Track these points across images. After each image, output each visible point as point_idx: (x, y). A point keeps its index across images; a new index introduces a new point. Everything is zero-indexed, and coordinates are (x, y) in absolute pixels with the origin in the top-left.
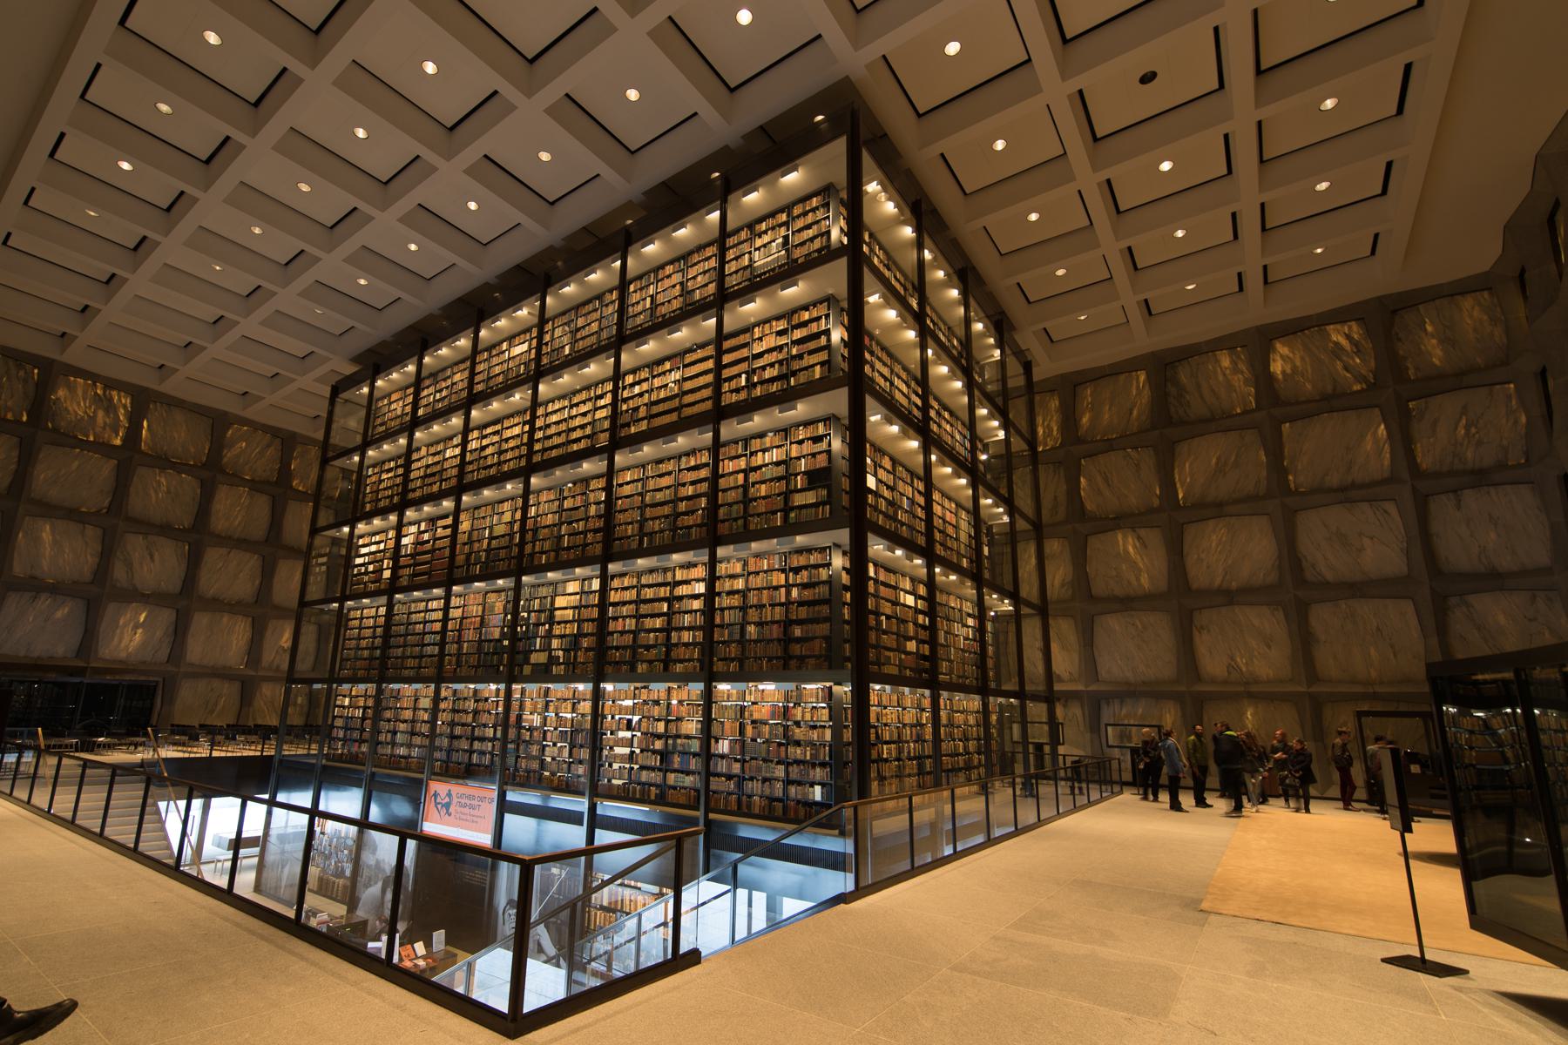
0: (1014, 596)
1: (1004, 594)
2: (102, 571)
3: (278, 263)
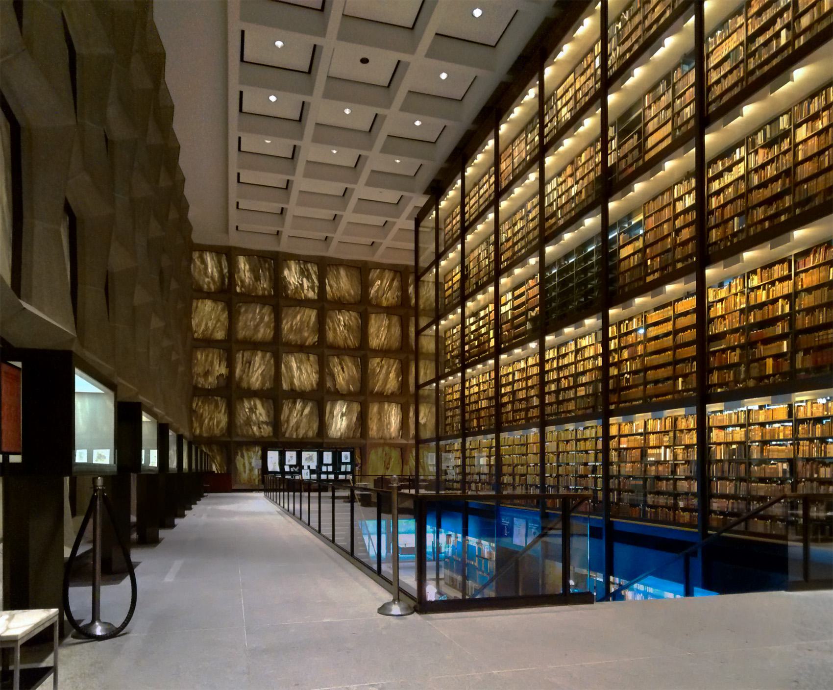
2: (321, 382)
3: (337, 196)
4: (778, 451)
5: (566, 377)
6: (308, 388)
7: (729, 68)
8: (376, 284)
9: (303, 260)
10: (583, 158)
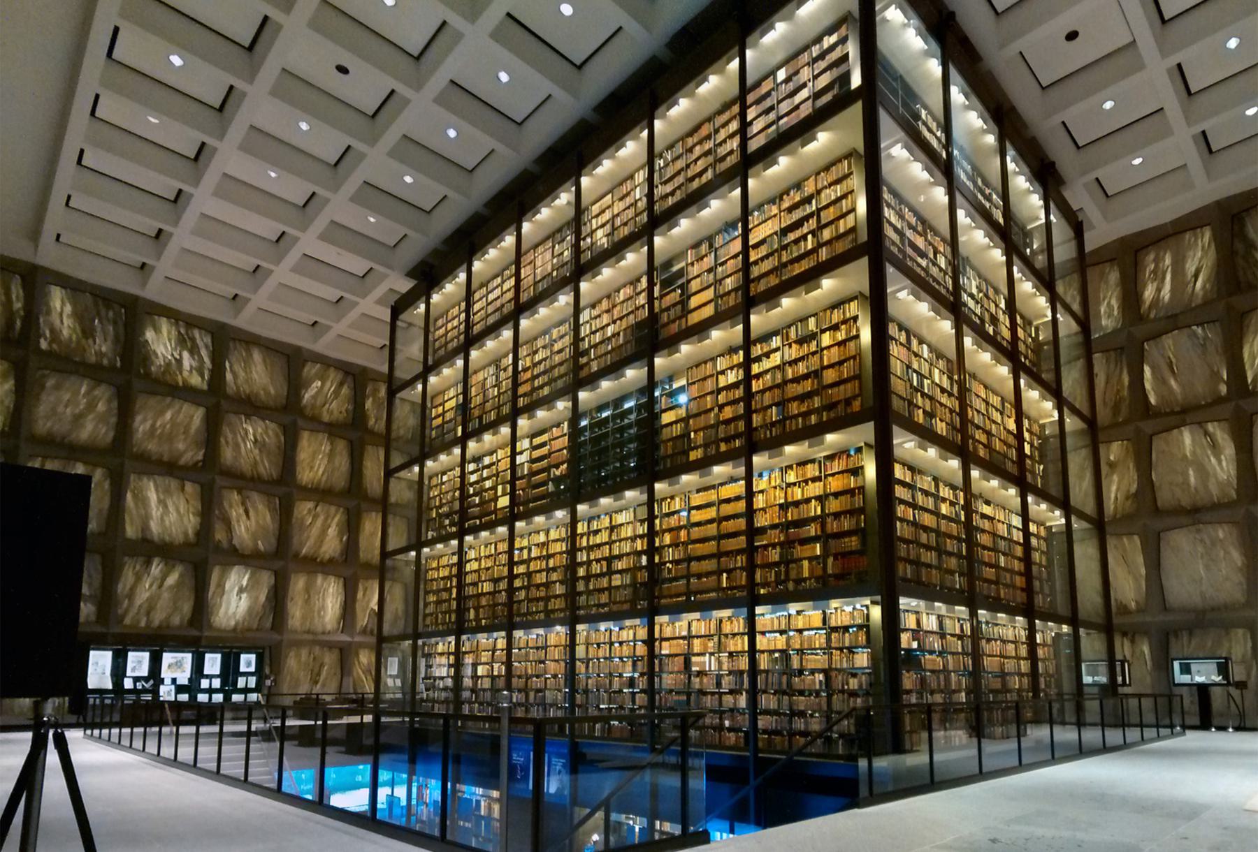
2: (204, 531)
5: (598, 561)
6: (179, 538)
8: (314, 385)
9: (186, 323)
10: (622, 296)
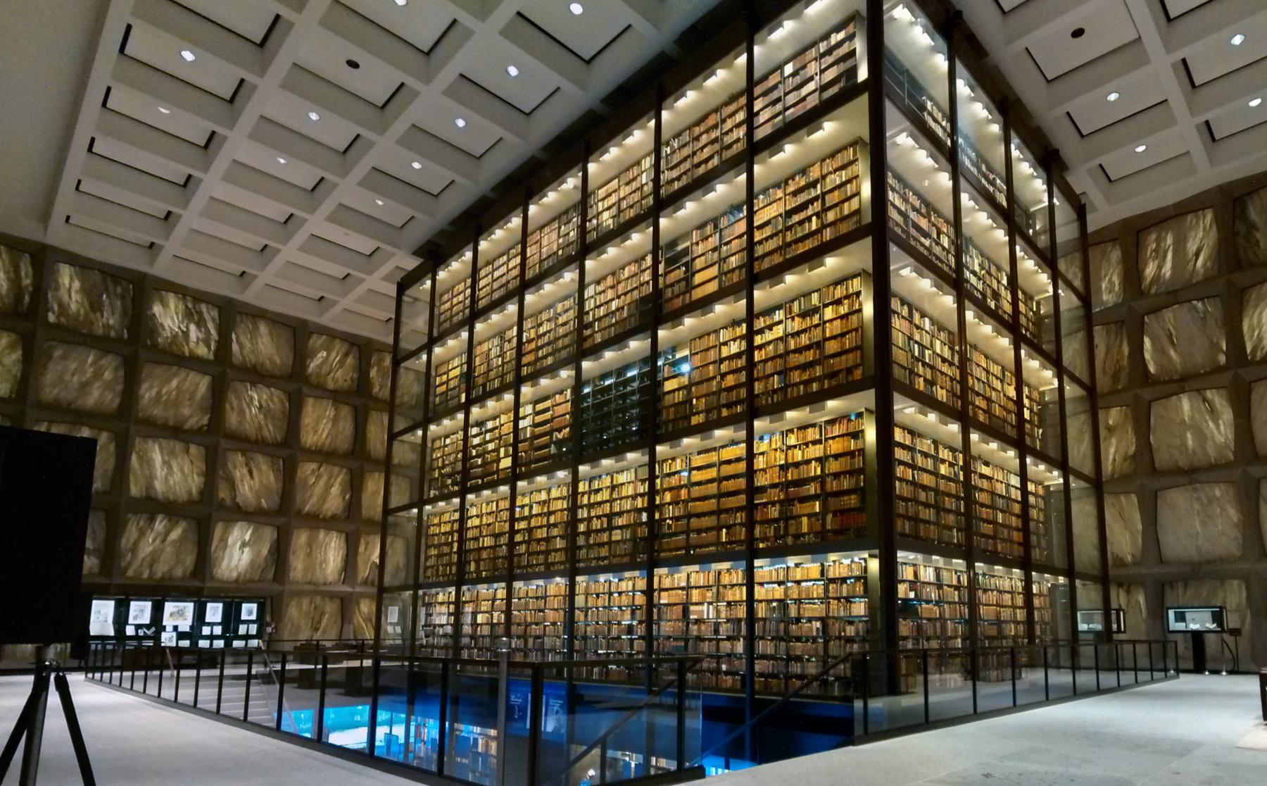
0: (1062, 464)
1: (1051, 462)
2: (208, 490)
4: (813, 609)
5: (598, 517)
7: (769, 233)
8: (320, 355)
9: (194, 298)
10: (627, 273)
